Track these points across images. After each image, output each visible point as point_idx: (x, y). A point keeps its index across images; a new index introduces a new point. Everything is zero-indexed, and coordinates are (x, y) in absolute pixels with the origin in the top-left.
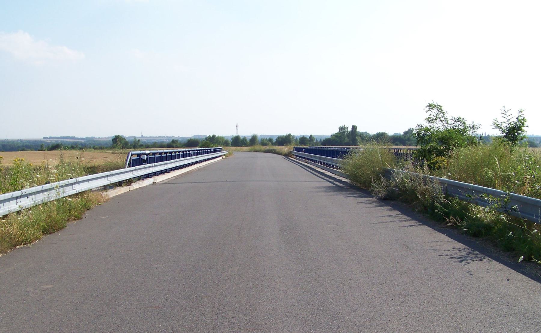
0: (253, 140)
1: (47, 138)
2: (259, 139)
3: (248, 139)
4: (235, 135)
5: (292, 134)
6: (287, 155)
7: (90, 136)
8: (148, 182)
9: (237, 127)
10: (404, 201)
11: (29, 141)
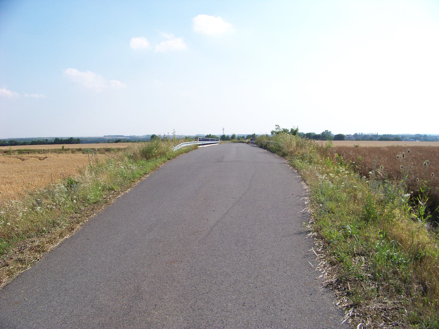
0: (233, 137)
1: (106, 136)
2: (236, 137)
3: (230, 137)
4: (222, 134)
5: (256, 134)
6: (248, 143)
7: (132, 135)
8: (202, 146)
9: (223, 129)
10: (262, 146)
11: (95, 138)
